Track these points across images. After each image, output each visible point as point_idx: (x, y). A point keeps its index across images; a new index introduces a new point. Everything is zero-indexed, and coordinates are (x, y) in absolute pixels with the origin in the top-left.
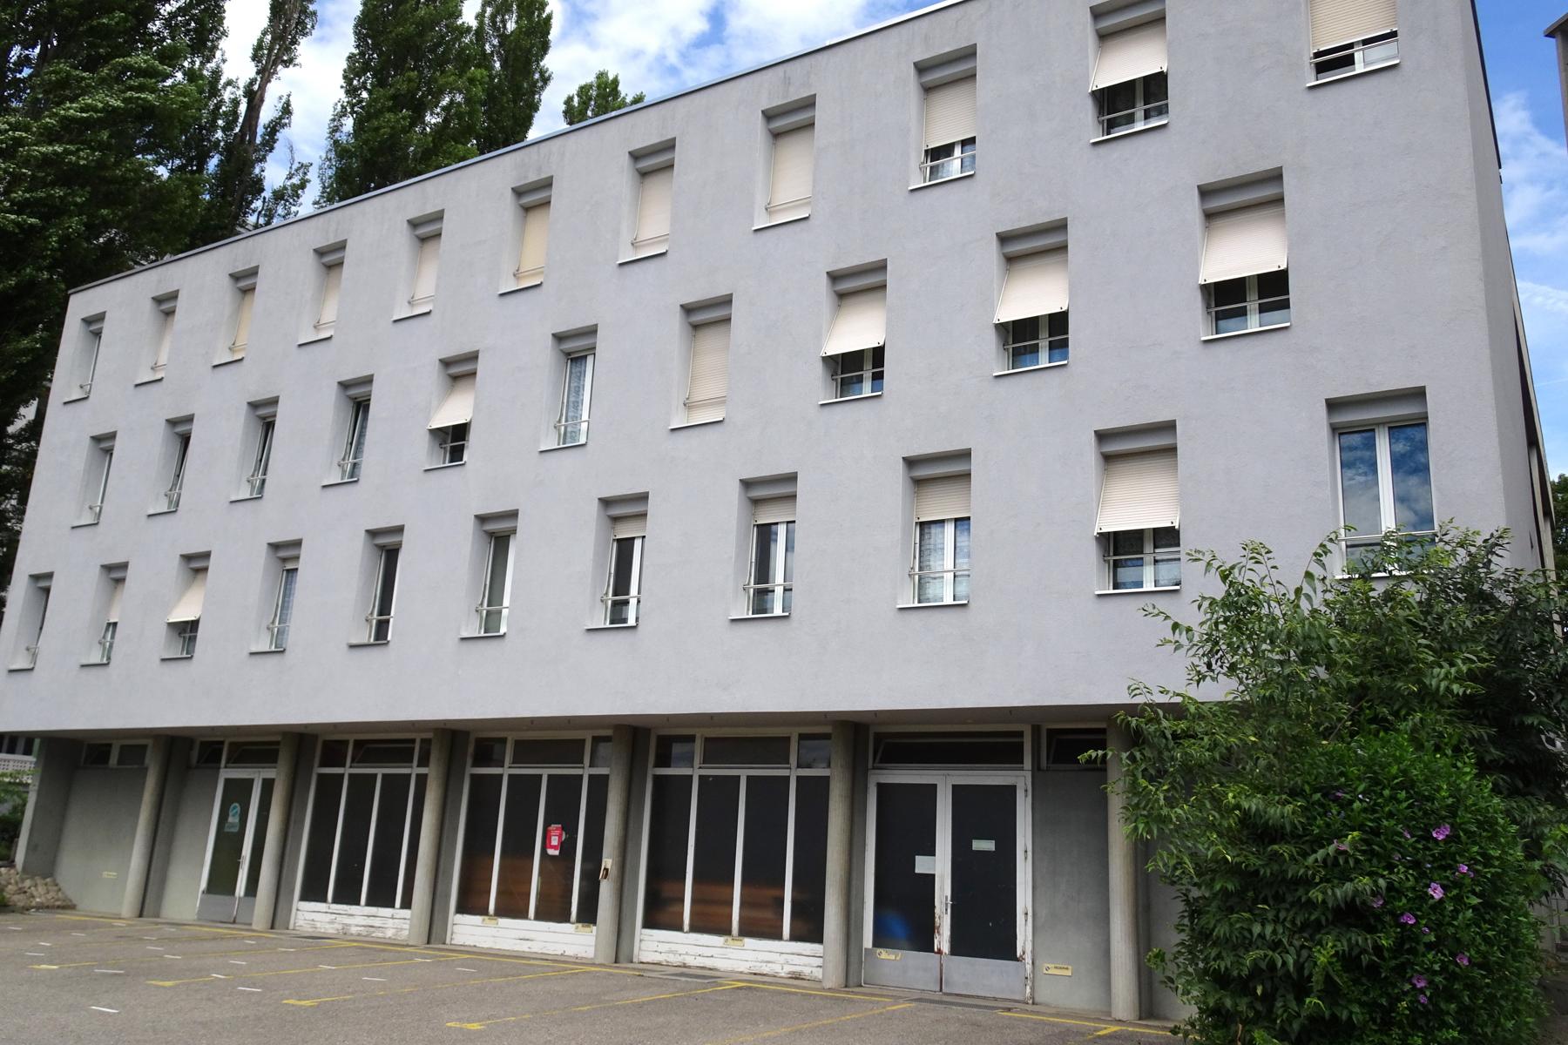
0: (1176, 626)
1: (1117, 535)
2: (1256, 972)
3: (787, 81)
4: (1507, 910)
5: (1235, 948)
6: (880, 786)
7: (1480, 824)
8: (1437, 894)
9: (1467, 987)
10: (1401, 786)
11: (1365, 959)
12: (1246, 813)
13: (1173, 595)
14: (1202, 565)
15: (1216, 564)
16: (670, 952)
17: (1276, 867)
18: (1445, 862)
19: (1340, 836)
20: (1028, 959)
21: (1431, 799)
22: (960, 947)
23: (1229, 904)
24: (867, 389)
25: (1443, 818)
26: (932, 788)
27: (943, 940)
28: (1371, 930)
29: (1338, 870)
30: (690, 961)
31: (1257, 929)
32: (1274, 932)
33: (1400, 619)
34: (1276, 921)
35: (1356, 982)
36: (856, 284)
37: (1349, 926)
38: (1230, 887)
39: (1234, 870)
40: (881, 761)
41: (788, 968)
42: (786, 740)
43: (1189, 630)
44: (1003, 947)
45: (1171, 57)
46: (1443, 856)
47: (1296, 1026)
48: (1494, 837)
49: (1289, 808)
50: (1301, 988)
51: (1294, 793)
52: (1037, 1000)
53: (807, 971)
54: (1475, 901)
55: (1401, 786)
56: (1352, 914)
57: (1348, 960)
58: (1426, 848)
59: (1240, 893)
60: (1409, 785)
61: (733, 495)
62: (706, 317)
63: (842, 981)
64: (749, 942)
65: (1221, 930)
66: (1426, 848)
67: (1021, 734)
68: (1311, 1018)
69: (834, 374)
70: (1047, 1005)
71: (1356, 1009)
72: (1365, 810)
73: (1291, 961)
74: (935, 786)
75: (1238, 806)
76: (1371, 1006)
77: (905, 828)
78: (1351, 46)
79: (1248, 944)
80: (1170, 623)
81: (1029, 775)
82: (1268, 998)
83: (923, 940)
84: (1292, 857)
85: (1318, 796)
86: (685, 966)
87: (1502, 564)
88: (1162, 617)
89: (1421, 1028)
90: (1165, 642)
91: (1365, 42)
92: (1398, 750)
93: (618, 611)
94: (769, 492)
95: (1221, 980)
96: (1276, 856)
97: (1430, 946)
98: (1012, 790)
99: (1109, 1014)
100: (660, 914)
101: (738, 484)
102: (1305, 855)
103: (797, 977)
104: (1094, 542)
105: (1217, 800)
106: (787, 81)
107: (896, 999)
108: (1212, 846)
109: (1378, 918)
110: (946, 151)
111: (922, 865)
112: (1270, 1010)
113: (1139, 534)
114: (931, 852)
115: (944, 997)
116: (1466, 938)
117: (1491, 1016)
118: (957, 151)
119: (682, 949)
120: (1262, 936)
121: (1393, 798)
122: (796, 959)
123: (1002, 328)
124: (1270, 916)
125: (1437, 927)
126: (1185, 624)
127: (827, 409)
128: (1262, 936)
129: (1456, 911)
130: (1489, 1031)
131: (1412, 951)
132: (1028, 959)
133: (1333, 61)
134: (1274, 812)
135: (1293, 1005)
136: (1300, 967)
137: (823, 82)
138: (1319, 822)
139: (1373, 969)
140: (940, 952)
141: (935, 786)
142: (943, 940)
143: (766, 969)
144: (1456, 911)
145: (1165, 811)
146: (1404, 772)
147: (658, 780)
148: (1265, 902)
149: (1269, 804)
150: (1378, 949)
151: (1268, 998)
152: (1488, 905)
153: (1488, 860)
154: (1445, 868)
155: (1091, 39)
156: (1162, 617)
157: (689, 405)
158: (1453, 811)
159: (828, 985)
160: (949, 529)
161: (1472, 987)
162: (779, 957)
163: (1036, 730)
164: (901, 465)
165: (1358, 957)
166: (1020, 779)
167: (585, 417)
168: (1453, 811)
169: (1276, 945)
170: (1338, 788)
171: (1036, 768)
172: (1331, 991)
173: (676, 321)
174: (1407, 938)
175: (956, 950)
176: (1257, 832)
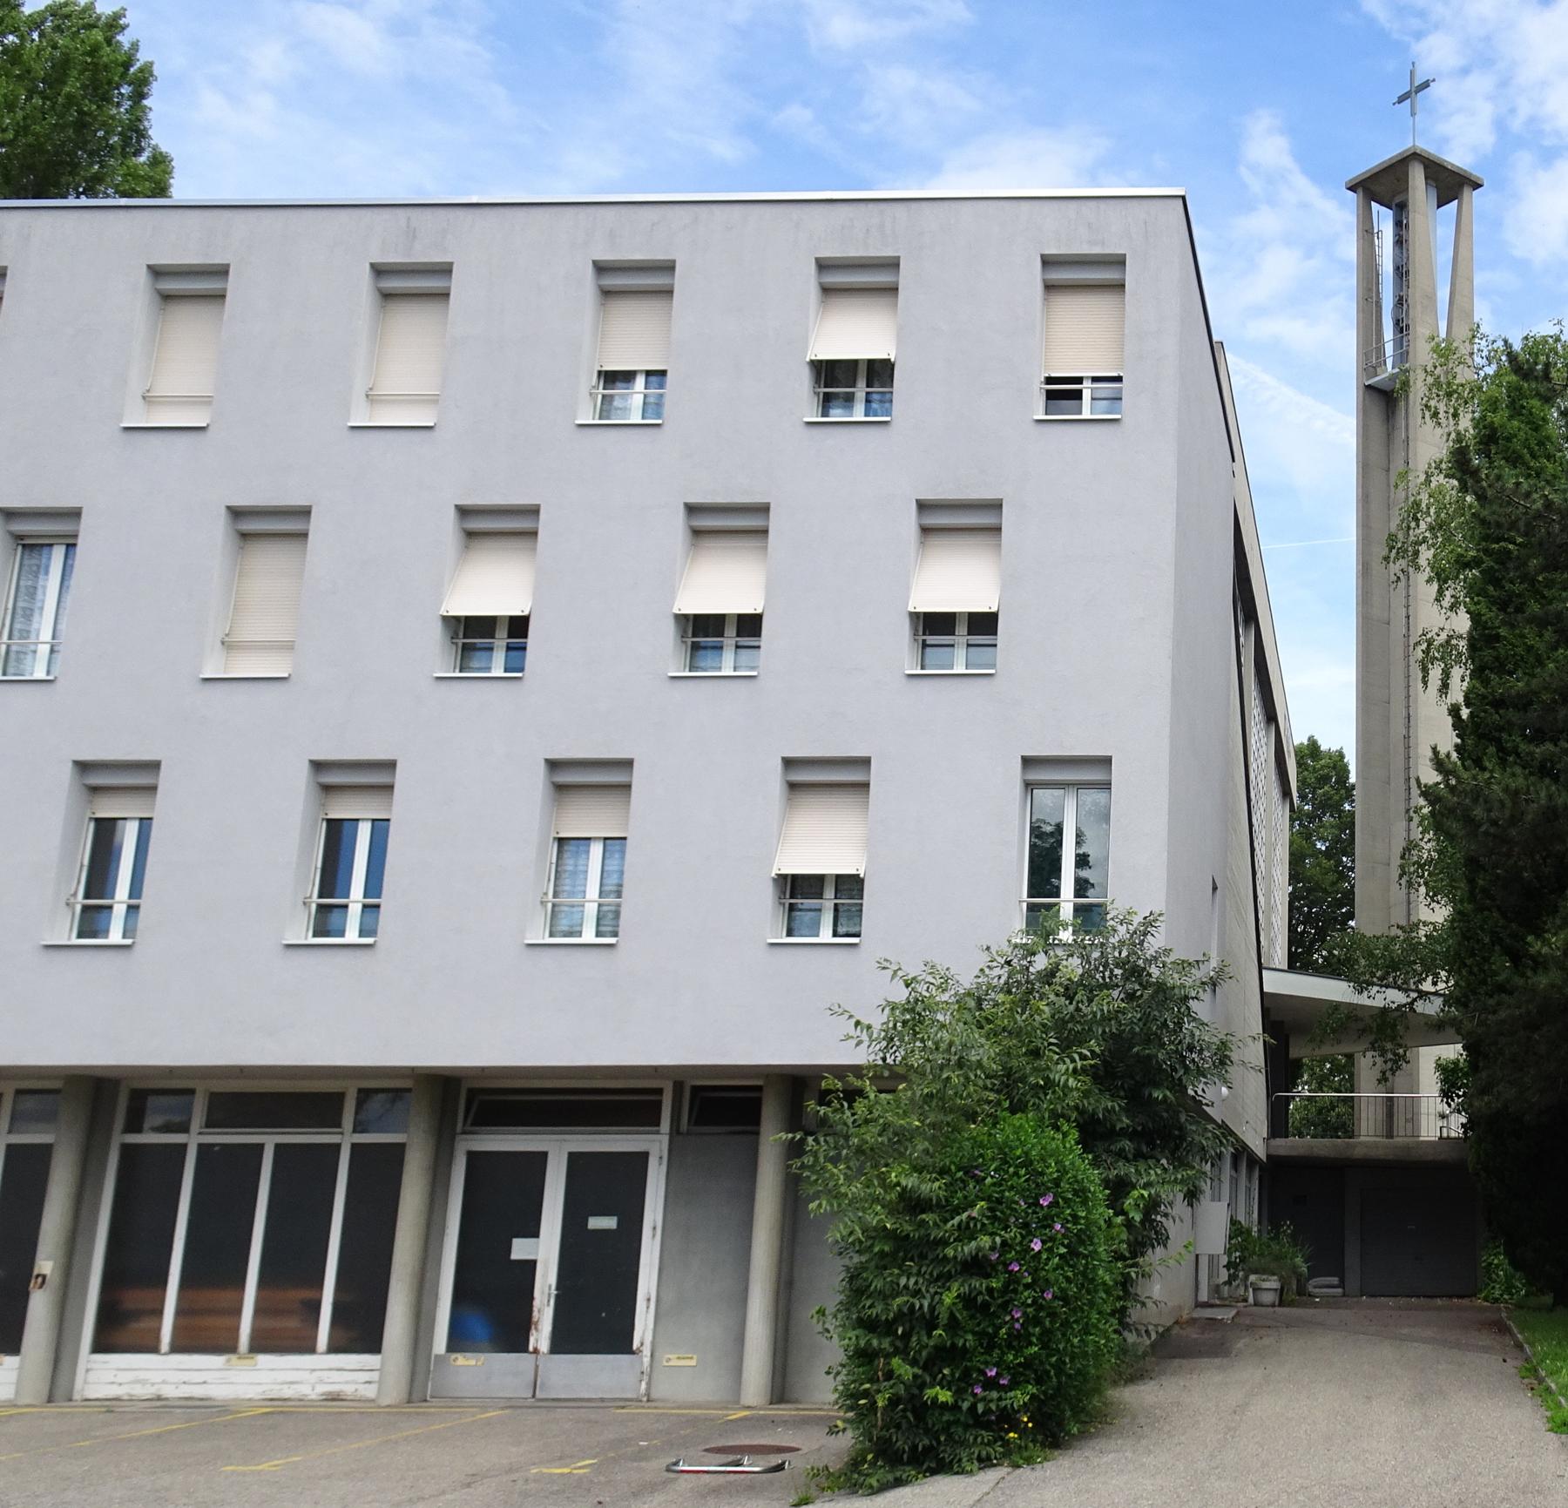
0: (858, 1023)
1: (794, 877)
2: (900, 1316)
3: (412, 234)
4: (1085, 1257)
5: (885, 1298)
6: (472, 1156)
7: (1076, 1192)
8: (1037, 1246)
9: (1049, 1315)
10: (1022, 1165)
11: (980, 1299)
12: (904, 1189)
13: (851, 949)
14: (889, 973)
15: (900, 973)
16: (137, 1381)
17: (922, 1231)
18: (1046, 1222)
19: (973, 1205)
20: (647, 1351)
21: (1042, 1174)
22: (563, 1342)
23: (883, 1262)
24: (499, 659)
25: (1049, 1189)
26: (543, 1156)
27: (541, 1337)
28: (987, 1276)
29: (967, 1232)
30: (169, 1391)
31: (903, 1281)
32: (916, 1283)
33: (1036, 1024)
34: (919, 1274)
35: (972, 1317)
36: (494, 526)
37: (972, 1275)
38: (887, 1249)
39: (891, 1235)
40: (473, 1125)
41: (322, 1389)
42: (340, 1097)
43: (869, 1027)
44: (617, 1339)
45: (900, 342)
46: (1045, 1218)
47: (924, 1354)
48: (1084, 1202)
49: (937, 1184)
50: (931, 1325)
51: (943, 1172)
52: (653, 1396)
53: (348, 1389)
54: (1063, 1250)
55: (1022, 1165)
56: (976, 1266)
57: (967, 1301)
58: (1034, 1212)
59: (894, 1254)
60: (1028, 1163)
61: (300, 779)
62: (267, 527)
63: (404, 1396)
64: (264, 1360)
65: (878, 1284)
66: (1034, 1212)
67: (659, 1091)
68: (935, 1347)
69: (454, 636)
70: (663, 1401)
71: (970, 1337)
72: (994, 1184)
73: (926, 1304)
74: (544, 1155)
75: (898, 1184)
76: (980, 1335)
77: (501, 1202)
78: (1079, 380)
79: (896, 1293)
80: (853, 1021)
81: (665, 1139)
82: (906, 1336)
83: (513, 1337)
84: (935, 1224)
85: (960, 1174)
86: (159, 1398)
87: (1154, 944)
88: (846, 1015)
89: (1013, 1348)
90: (849, 1037)
91: (1095, 379)
92: (1021, 1132)
93: (92, 921)
94: (350, 784)
95: (869, 1325)
96: (923, 1223)
97: (1027, 1286)
98: (644, 1156)
99: (738, 1402)
100: (120, 1329)
101: (306, 765)
102: (946, 1221)
103: (334, 1398)
104: (771, 883)
105: (883, 1179)
106: (412, 234)
107: (484, 1409)
108: (877, 1216)
109: (993, 1266)
110: (627, 377)
111: (520, 1249)
112: (906, 1346)
113: (820, 879)
114: (535, 1234)
115: (537, 1400)
116: (1052, 1277)
117: (1064, 1335)
118: (640, 381)
119: (155, 1377)
120: (906, 1287)
121: (1016, 1174)
122: (336, 1376)
123: (682, 619)
124: (914, 1270)
125: (1034, 1272)
126: (865, 1022)
127: (444, 685)
128: (906, 1287)
129: (1048, 1259)
130: (1061, 1347)
131: (1015, 1291)
132: (647, 1351)
133: (1062, 393)
134: (925, 1188)
135: (925, 1339)
136: (932, 1308)
137: (463, 246)
138: (960, 1195)
139: (986, 1305)
140: (536, 1351)
141: (544, 1155)
142: (541, 1337)
143: (288, 1392)
144: (1048, 1259)
145: (843, 1190)
146: (1026, 1154)
147: (126, 1149)
148: (912, 1260)
149: (922, 1181)
150: (990, 1290)
151: (906, 1336)
152: (1073, 1252)
153: (1075, 1218)
154: (1045, 1227)
155: (813, 291)
156: (846, 1015)
157: (228, 645)
158: (1057, 1182)
159: (386, 1401)
160: (596, 850)
161: (1053, 1315)
162: (318, 1373)
163: (678, 1087)
164: (541, 769)
165: (975, 1298)
166: (655, 1145)
167: (46, 635)
168: (1057, 1182)
169: (917, 1293)
170: (976, 1168)
171: (675, 1132)
172: (953, 1325)
173: (219, 527)
174: (1013, 1279)
175: (558, 1346)
176: (912, 1204)
